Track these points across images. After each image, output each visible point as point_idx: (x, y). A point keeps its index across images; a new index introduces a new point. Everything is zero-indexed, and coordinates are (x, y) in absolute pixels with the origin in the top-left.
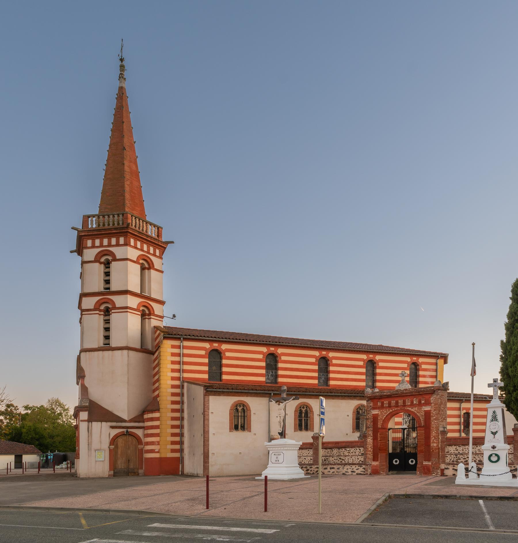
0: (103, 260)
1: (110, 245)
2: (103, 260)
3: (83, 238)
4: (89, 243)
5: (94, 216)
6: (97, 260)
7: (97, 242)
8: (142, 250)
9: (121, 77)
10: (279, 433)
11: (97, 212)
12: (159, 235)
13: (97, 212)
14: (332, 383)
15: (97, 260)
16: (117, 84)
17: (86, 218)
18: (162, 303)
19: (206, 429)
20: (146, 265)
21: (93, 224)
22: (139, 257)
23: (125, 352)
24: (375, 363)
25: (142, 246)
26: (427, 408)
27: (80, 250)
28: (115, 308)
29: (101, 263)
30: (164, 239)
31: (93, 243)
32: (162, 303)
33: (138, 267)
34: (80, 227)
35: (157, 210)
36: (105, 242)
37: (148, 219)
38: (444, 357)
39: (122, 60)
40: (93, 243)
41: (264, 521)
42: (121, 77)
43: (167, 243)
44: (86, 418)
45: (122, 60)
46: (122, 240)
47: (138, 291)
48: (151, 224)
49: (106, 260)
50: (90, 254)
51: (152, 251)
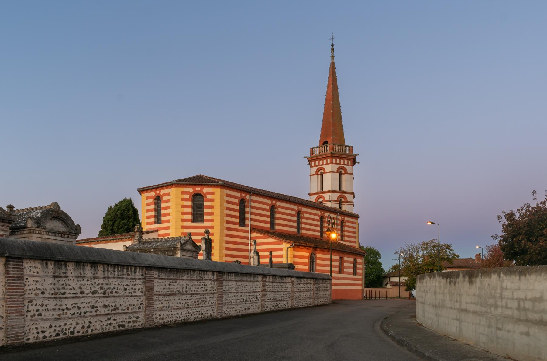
0: (319, 173)
1: (323, 165)
2: (319, 173)
3: (311, 160)
5: (317, 147)
8: (340, 164)
10: (470, 282)
11: (318, 145)
12: (352, 151)
14: (307, 254)
15: (317, 173)
16: (330, 60)
17: (312, 149)
19: (115, 260)
20: (341, 172)
21: (317, 152)
22: (338, 169)
23: (330, 174)
25: (340, 161)
26: (371, 266)
29: (318, 175)
31: (315, 164)
33: (338, 174)
34: (309, 155)
35: (350, 139)
36: (321, 162)
39: (333, 45)
45: (333, 45)
46: (329, 161)
47: (338, 189)
48: (348, 146)
49: (320, 173)
51: (346, 163)
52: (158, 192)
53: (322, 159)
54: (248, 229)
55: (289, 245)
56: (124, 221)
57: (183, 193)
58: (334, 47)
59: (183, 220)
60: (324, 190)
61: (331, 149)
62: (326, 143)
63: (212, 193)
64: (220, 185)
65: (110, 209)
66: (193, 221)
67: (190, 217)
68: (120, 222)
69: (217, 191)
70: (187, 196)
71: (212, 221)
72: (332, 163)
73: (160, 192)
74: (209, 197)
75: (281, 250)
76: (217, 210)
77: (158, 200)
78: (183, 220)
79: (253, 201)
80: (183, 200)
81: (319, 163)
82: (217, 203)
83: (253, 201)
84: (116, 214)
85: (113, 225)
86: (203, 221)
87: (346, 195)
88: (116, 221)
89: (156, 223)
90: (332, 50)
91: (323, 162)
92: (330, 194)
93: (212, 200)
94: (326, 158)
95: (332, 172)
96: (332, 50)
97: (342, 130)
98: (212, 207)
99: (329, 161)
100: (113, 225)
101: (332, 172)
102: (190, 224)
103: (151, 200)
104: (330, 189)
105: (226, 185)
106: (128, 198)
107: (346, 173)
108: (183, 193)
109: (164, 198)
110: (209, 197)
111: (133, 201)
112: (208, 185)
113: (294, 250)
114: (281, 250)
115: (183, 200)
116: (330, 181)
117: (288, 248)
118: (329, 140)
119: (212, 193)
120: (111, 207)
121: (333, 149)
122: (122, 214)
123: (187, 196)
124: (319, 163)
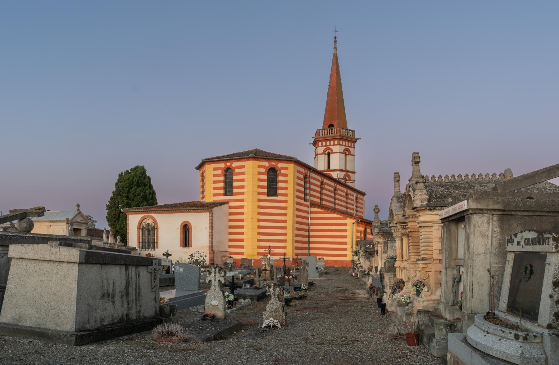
1: (330, 145)
2: (326, 153)
4: (320, 144)
6: (324, 153)
7: (324, 143)
8: (345, 146)
9: (336, 48)
11: (322, 128)
12: (354, 135)
13: (322, 128)
15: (324, 153)
16: (332, 52)
18: (354, 173)
20: (347, 153)
22: (345, 150)
23: (338, 154)
24: (161, 309)
27: (315, 144)
28: (332, 153)
30: (356, 137)
31: (322, 144)
32: (354, 173)
35: (352, 123)
36: (328, 143)
37: (349, 128)
38: (363, 194)
39: (335, 38)
40: (322, 144)
41: (465, 238)
42: (336, 48)
43: (357, 139)
44: (77, 259)
45: (335, 38)
46: (336, 142)
48: (350, 130)
50: (320, 150)
52: (228, 164)
53: (330, 140)
54: (308, 203)
55: (354, 221)
56: (140, 188)
57: (259, 167)
58: (337, 39)
59: (259, 194)
60: (331, 168)
61: (338, 131)
62: (331, 126)
63: (286, 169)
64: (252, 157)
65: (120, 175)
66: (269, 194)
67: (265, 191)
68: (136, 189)
69: (291, 167)
70: (263, 170)
71: (286, 195)
72: (339, 144)
73: (231, 164)
74: (283, 172)
75: (345, 224)
76: (290, 186)
77: (228, 173)
78: (259, 194)
79: (312, 178)
80: (260, 173)
81: (326, 143)
82: (291, 179)
83: (312, 178)
84: (132, 181)
85: (128, 192)
86: (276, 195)
87: (350, 174)
88: (131, 188)
89: (225, 194)
90: (335, 42)
91: (330, 143)
92: (338, 172)
93: (286, 175)
94: (334, 140)
95: (340, 153)
96: (335, 42)
97: (345, 115)
98: (286, 182)
99: (336, 142)
100: (128, 192)
101: (340, 153)
102: (265, 197)
103: (220, 172)
104: (337, 168)
105: (298, 163)
106: (141, 165)
107: (350, 154)
108: (259, 167)
109: (237, 171)
110: (283, 172)
111: (145, 168)
112: (235, 159)
113: (357, 226)
114: (345, 224)
115: (260, 173)
116: (336, 161)
117: (353, 223)
118: (335, 124)
119: (286, 169)
120: (122, 173)
121: (340, 132)
122: (138, 182)
123: (263, 170)
124: (326, 143)
